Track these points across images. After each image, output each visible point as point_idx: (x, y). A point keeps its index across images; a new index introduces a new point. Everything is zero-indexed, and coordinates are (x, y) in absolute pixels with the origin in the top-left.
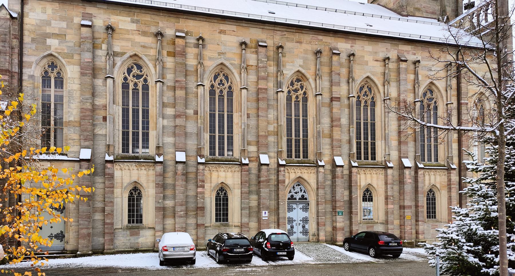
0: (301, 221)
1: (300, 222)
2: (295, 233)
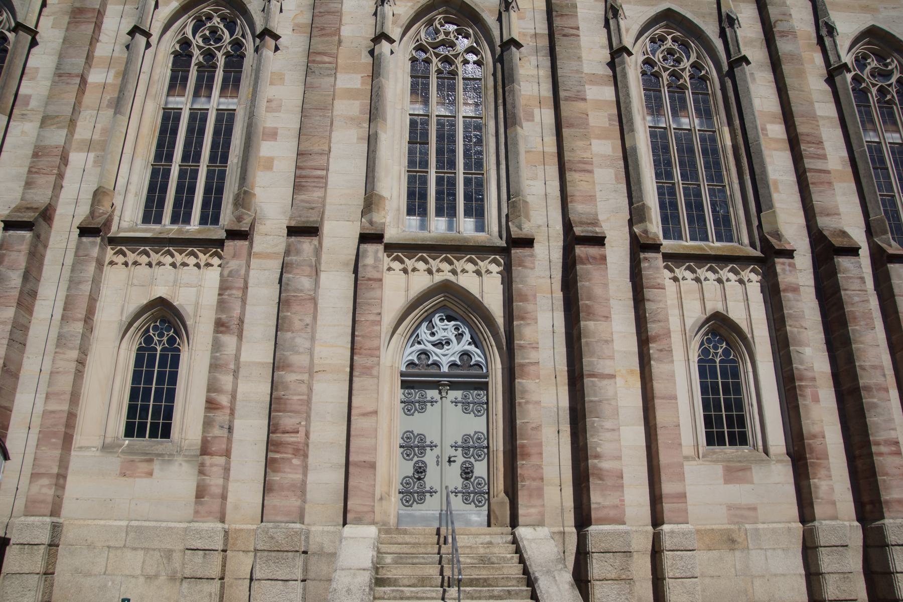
0: (455, 447)
1: (452, 452)
2: (432, 492)
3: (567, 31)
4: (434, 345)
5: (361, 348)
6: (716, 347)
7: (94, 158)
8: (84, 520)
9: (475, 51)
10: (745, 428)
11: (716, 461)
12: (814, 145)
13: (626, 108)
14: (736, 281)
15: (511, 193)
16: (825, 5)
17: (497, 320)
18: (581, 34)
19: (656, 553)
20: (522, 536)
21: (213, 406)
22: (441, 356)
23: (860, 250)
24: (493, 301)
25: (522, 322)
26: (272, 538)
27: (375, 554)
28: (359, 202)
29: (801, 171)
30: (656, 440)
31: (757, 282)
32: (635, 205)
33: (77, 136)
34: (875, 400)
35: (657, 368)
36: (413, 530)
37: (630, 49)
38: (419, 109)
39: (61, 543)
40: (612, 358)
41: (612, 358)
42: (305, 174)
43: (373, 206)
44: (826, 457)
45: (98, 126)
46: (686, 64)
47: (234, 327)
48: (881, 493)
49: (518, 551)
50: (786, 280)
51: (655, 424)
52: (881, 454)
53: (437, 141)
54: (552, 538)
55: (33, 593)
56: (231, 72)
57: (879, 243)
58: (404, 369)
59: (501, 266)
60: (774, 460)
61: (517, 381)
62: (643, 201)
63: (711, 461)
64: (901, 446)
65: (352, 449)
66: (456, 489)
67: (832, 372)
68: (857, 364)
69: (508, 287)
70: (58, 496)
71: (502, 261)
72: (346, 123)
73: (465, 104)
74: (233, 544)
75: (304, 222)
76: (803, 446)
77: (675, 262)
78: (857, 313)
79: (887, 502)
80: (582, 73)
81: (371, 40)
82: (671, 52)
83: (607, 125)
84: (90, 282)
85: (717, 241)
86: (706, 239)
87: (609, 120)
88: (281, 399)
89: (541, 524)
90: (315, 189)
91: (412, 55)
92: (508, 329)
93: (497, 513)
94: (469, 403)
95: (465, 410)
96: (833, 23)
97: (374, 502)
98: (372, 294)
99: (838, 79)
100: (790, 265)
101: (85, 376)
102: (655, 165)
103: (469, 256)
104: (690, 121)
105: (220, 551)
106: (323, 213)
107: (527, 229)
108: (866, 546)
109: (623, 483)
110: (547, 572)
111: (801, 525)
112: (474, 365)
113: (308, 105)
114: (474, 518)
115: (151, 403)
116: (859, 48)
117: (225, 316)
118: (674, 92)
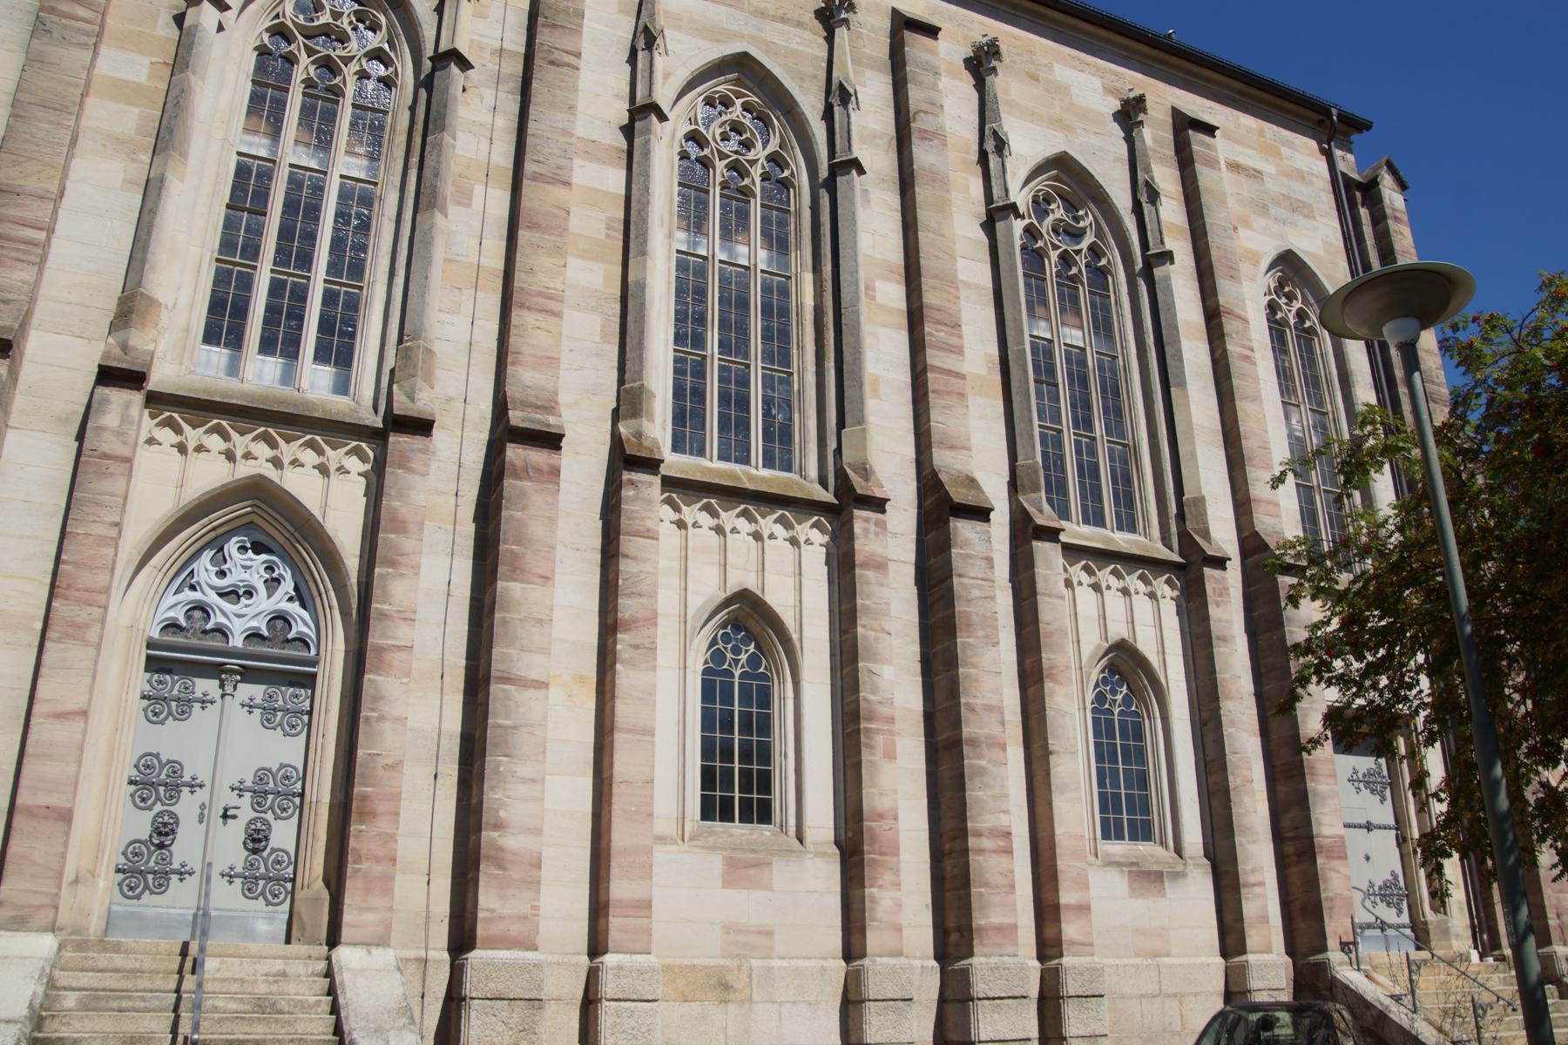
0: (239, 790)
1: (232, 799)
2: (183, 873)
3: (557, 55)
4: (221, 595)
5: (69, 587)
6: (736, 651)
9: (287, 33)
10: (770, 794)
11: (713, 848)
12: (944, 328)
13: (639, 212)
14: (785, 540)
15: (406, 332)
16: (997, 103)
17: (345, 560)
18: (582, 65)
19: (589, 1004)
20: (343, 964)
22: (232, 617)
23: (992, 513)
24: (345, 530)
25: (390, 570)
27: (40, 989)
28: (108, 304)
29: (919, 368)
30: (610, 804)
31: (821, 545)
32: (627, 386)
34: (983, 763)
35: (625, 676)
36: (133, 945)
37: (665, 109)
38: (259, 146)
40: (546, 651)
41: (546, 651)
43: (134, 316)
44: (896, 852)
46: (759, 153)
48: (973, 915)
49: (331, 991)
50: (867, 548)
51: (611, 776)
52: (981, 851)
53: (283, 213)
54: (399, 969)
57: (1025, 505)
58: (155, 634)
59: (368, 462)
60: (810, 852)
61: (367, 677)
62: (641, 379)
63: (703, 847)
64: (1013, 840)
65: (24, 781)
66: (232, 869)
67: (924, 711)
68: (963, 700)
69: (375, 502)
71: (371, 454)
72: (105, 146)
73: (349, 153)
76: (859, 832)
77: (685, 495)
78: (974, 617)
79: (981, 929)
80: (572, 135)
82: (737, 128)
83: (602, 236)
85: (764, 466)
86: (745, 460)
87: (607, 228)
89: (383, 942)
90: (17, 264)
91: (262, 41)
92: (364, 580)
93: (305, 917)
94: (275, 709)
95: (267, 723)
96: (1006, 135)
97: (60, 887)
98: (105, 485)
99: (1000, 226)
100: (877, 523)
102: (676, 320)
103: (309, 437)
104: (754, 254)
106: (28, 314)
107: (424, 401)
108: (942, 1001)
109: (540, 877)
110: (376, 1031)
111: (844, 964)
112: (295, 639)
113: (28, 96)
114: (262, 926)
116: (1040, 183)
118: (731, 198)
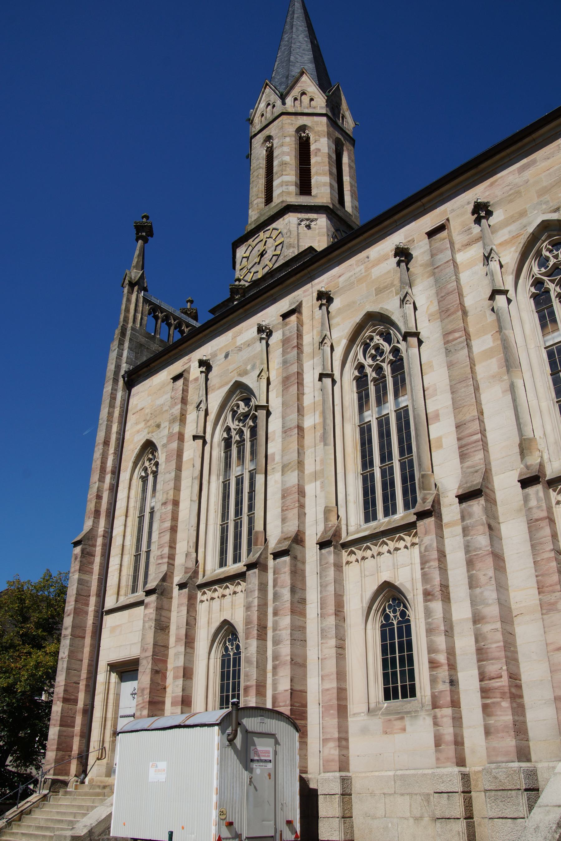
7: (320, 484)
8: (365, 772)
21: (435, 665)
26: (496, 778)
33: (307, 472)
39: (353, 792)
42: (465, 443)
45: (318, 459)
47: (438, 594)
55: (337, 832)
56: (543, 310)
70: (343, 755)
74: (475, 786)
75: (471, 487)
81: (489, 300)
84: (333, 583)
88: (483, 649)
90: (475, 453)
101: (347, 656)
105: (460, 793)
115: (398, 669)
117: (429, 586)
